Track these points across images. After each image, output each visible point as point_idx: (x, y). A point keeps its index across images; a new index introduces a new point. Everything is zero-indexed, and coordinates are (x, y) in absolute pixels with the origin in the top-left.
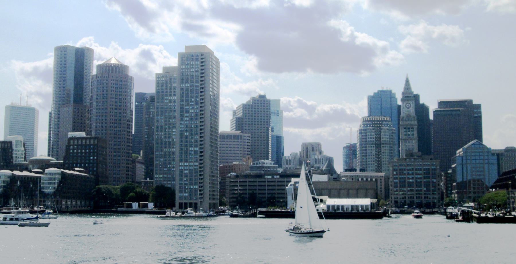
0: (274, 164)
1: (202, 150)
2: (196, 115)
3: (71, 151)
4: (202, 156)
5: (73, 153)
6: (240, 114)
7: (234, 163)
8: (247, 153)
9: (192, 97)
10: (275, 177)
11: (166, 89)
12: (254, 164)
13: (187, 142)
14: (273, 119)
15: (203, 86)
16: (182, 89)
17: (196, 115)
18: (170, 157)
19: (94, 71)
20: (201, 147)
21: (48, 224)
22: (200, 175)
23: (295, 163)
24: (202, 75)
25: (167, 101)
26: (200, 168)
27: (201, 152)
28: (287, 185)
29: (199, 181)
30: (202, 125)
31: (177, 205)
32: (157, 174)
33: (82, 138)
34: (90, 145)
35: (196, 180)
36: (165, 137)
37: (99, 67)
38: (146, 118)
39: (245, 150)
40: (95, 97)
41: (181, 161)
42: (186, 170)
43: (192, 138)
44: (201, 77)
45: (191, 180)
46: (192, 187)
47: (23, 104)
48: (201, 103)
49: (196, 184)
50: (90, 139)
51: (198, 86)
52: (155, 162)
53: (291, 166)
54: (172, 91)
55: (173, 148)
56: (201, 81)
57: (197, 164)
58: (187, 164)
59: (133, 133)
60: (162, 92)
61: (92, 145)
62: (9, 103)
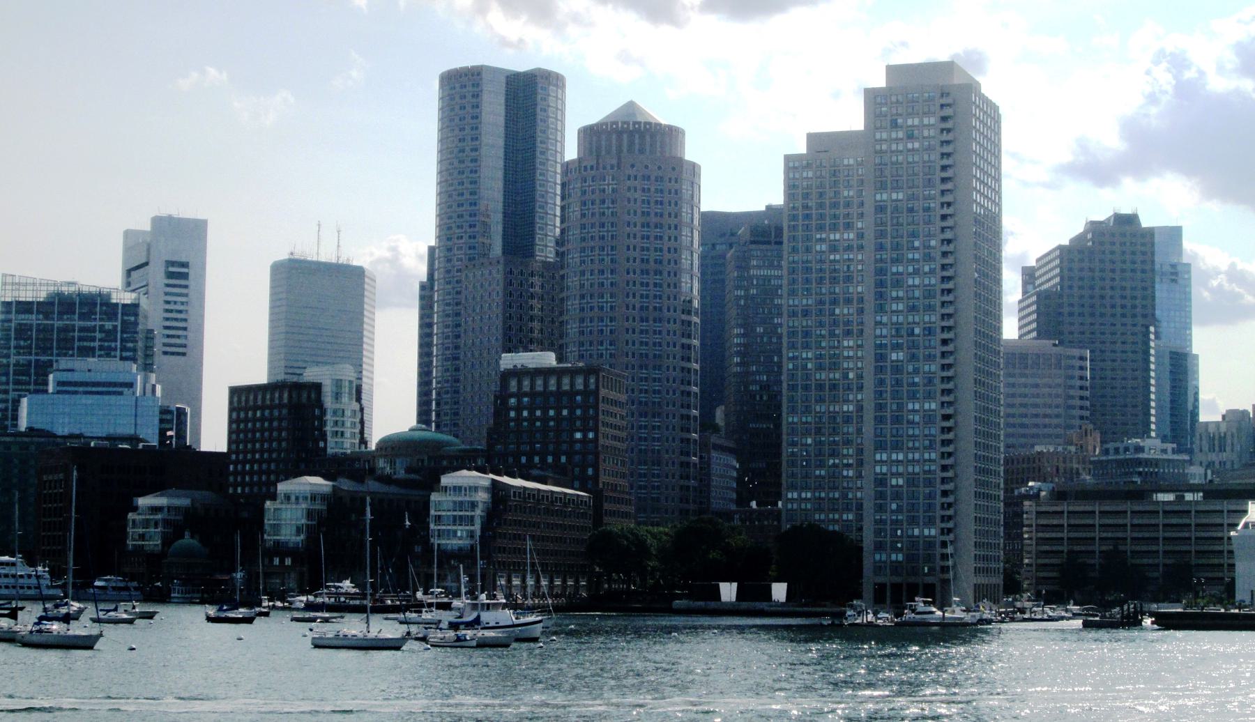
0: (1174, 452)
1: (950, 411)
2: (929, 294)
3: (512, 414)
4: (949, 429)
5: (519, 419)
6: (1050, 281)
7: (1038, 448)
8: (1077, 412)
9: (914, 235)
10: (1189, 497)
11: (821, 206)
12: (1106, 452)
13: (898, 383)
14: (1161, 291)
15: (948, 198)
16: (880, 209)
17: (929, 294)
18: (835, 432)
19: (571, 151)
20: (946, 399)
21: (155, 613)
22: (945, 493)
23: (1238, 448)
24: (945, 162)
25: (824, 247)
26: (944, 468)
27: (946, 417)
28: (1233, 526)
29: (939, 513)
30: (950, 328)
31: (868, 590)
32: (793, 487)
33: (545, 372)
34: (572, 393)
35: (930, 507)
36: (820, 368)
37: (590, 135)
38: (738, 298)
39: (1070, 402)
40: (575, 233)
41: (880, 446)
42: (898, 475)
43: (916, 371)
44: (944, 168)
45: (913, 507)
46: (916, 532)
47: (326, 254)
48: (945, 254)
49: (930, 522)
50: (573, 373)
51: (930, 198)
52: (786, 450)
53: (1224, 456)
54: (842, 211)
55: (847, 401)
56: (944, 180)
57: (933, 456)
58: (901, 457)
59: (1010, 329)
60: (808, 217)
61: (578, 393)
62: (283, 256)
